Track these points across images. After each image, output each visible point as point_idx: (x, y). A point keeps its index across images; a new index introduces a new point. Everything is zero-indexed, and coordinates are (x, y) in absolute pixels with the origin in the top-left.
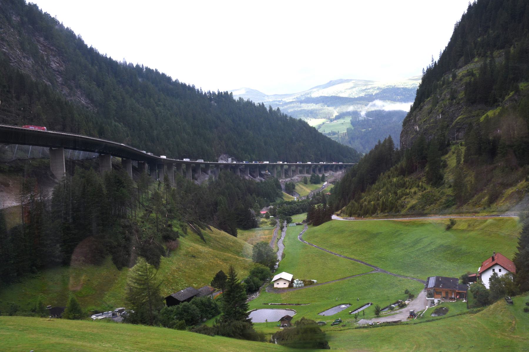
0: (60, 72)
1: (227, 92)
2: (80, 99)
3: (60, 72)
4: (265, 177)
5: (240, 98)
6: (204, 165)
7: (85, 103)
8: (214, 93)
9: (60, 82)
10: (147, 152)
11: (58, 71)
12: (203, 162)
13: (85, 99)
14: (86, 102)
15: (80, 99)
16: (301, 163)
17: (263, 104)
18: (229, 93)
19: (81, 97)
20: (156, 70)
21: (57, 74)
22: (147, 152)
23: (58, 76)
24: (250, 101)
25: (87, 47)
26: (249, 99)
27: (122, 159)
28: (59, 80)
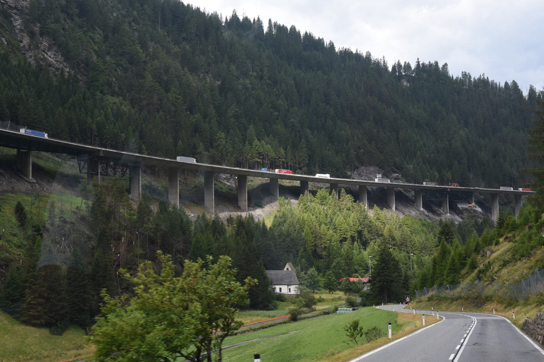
0: (18, 10)
1: (437, 63)
2: (47, 54)
3: (18, 10)
4: (466, 215)
5: (465, 75)
6: (299, 182)
7: (56, 61)
8: (408, 66)
9: (18, 26)
10: (516, 188)
11: (16, 8)
12: (329, 178)
13: (55, 55)
14: (57, 59)
15: (47, 54)
16: (389, 182)
17: (515, 84)
18: (440, 65)
19: (48, 51)
20: (293, 28)
21: (16, 14)
22: (516, 188)
23: (17, 17)
24: (486, 78)
25: (324, 43)
26: (483, 75)
27: (18, 152)
28: (17, 24)
